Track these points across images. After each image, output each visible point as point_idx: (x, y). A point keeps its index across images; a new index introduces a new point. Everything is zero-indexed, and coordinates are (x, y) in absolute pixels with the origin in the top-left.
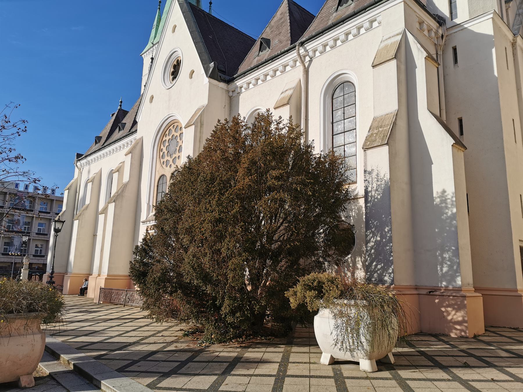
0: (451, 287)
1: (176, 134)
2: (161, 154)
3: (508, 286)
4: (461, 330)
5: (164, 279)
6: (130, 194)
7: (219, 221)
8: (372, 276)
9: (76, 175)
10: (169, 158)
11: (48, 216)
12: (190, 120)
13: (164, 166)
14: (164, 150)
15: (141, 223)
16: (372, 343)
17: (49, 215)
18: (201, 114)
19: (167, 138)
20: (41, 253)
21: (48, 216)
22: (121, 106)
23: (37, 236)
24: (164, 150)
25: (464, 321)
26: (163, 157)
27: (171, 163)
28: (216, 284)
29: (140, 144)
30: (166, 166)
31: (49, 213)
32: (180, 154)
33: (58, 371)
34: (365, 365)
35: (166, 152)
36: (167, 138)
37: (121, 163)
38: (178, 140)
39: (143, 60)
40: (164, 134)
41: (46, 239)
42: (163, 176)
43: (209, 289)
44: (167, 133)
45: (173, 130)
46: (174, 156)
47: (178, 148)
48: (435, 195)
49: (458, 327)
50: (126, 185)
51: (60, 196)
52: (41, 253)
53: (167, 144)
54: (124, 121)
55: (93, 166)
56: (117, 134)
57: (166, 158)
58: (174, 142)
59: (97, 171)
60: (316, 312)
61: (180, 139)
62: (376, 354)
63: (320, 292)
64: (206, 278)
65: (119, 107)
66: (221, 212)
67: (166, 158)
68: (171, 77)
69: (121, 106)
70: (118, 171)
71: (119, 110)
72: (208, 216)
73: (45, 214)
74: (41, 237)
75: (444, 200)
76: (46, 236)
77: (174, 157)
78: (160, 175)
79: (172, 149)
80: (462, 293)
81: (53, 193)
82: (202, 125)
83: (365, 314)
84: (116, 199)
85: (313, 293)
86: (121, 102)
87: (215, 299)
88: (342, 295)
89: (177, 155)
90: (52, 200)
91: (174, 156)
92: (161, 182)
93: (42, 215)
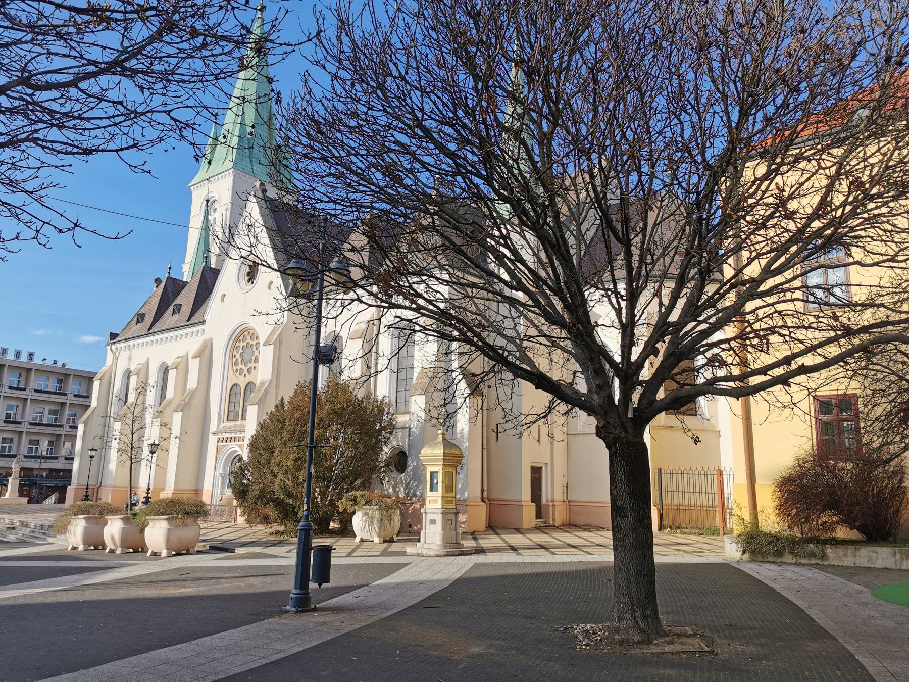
0: (462, 499)
1: (251, 342)
2: (234, 360)
3: (517, 498)
4: (464, 528)
5: (261, 496)
6: (198, 402)
7: (299, 459)
8: (409, 491)
9: (109, 362)
10: (243, 367)
11: (22, 394)
12: (269, 337)
13: (238, 374)
14: (238, 356)
15: (211, 435)
16: (380, 528)
17: (24, 392)
18: (280, 333)
19: (242, 344)
20: (9, 450)
21: (22, 394)
22: (169, 273)
23: (5, 425)
24: (238, 356)
25: (466, 522)
26: (236, 364)
27: (245, 372)
28: (295, 498)
29: (209, 347)
30: (240, 375)
31: (25, 390)
32: (256, 365)
33: (107, 598)
34: (376, 540)
35: (240, 360)
36: (242, 344)
37: (178, 357)
38: (254, 349)
39: (192, 194)
40: (238, 339)
41: (19, 430)
42: (236, 385)
43: (291, 501)
44: (241, 338)
45: (249, 337)
46: (249, 365)
47: (253, 358)
48: (458, 432)
49: (463, 526)
50: (193, 392)
51: (42, 363)
52: (9, 450)
53: (241, 351)
54: (177, 301)
55: (135, 352)
56: (169, 318)
57: (240, 366)
58: (249, 350)
59: (143, 361)
60: (354, 513)
61: (257, 349)
62: (382, 534)
63: (356, 502)
64: (289, 494)
65: (167, 275)
66: (299, 453)
67: (240, 366)
68: (247, 278)
69: (169, 273)
70: (176, 368)
71: (168, 278)
72: (292, 456)
73: (18, 392)
74: (12, 427)
75: (462, 437)
76: (19, 426)
77: (248, 367)
78: (233, 383)
79: (247, 357)
80: (467, 503)
81: (31, 359)
82: (281, 344)
83: (377, 512)
84: (183, 408)
85: (351, 503)
86: (170, 268)
87: (295, 507)
88: (366, 503)
89: (252, 365)
90: (29, 370)
91: (249, 365)
92: (233, 391)
93: (14, 393)
